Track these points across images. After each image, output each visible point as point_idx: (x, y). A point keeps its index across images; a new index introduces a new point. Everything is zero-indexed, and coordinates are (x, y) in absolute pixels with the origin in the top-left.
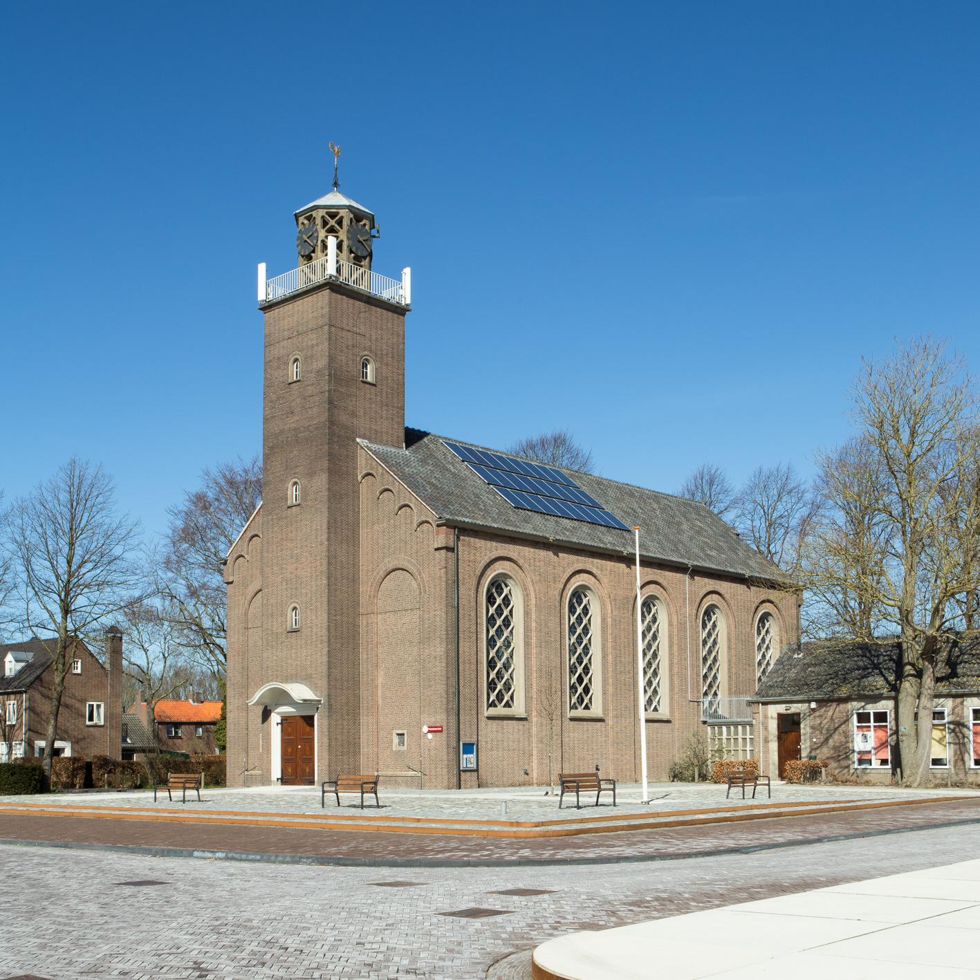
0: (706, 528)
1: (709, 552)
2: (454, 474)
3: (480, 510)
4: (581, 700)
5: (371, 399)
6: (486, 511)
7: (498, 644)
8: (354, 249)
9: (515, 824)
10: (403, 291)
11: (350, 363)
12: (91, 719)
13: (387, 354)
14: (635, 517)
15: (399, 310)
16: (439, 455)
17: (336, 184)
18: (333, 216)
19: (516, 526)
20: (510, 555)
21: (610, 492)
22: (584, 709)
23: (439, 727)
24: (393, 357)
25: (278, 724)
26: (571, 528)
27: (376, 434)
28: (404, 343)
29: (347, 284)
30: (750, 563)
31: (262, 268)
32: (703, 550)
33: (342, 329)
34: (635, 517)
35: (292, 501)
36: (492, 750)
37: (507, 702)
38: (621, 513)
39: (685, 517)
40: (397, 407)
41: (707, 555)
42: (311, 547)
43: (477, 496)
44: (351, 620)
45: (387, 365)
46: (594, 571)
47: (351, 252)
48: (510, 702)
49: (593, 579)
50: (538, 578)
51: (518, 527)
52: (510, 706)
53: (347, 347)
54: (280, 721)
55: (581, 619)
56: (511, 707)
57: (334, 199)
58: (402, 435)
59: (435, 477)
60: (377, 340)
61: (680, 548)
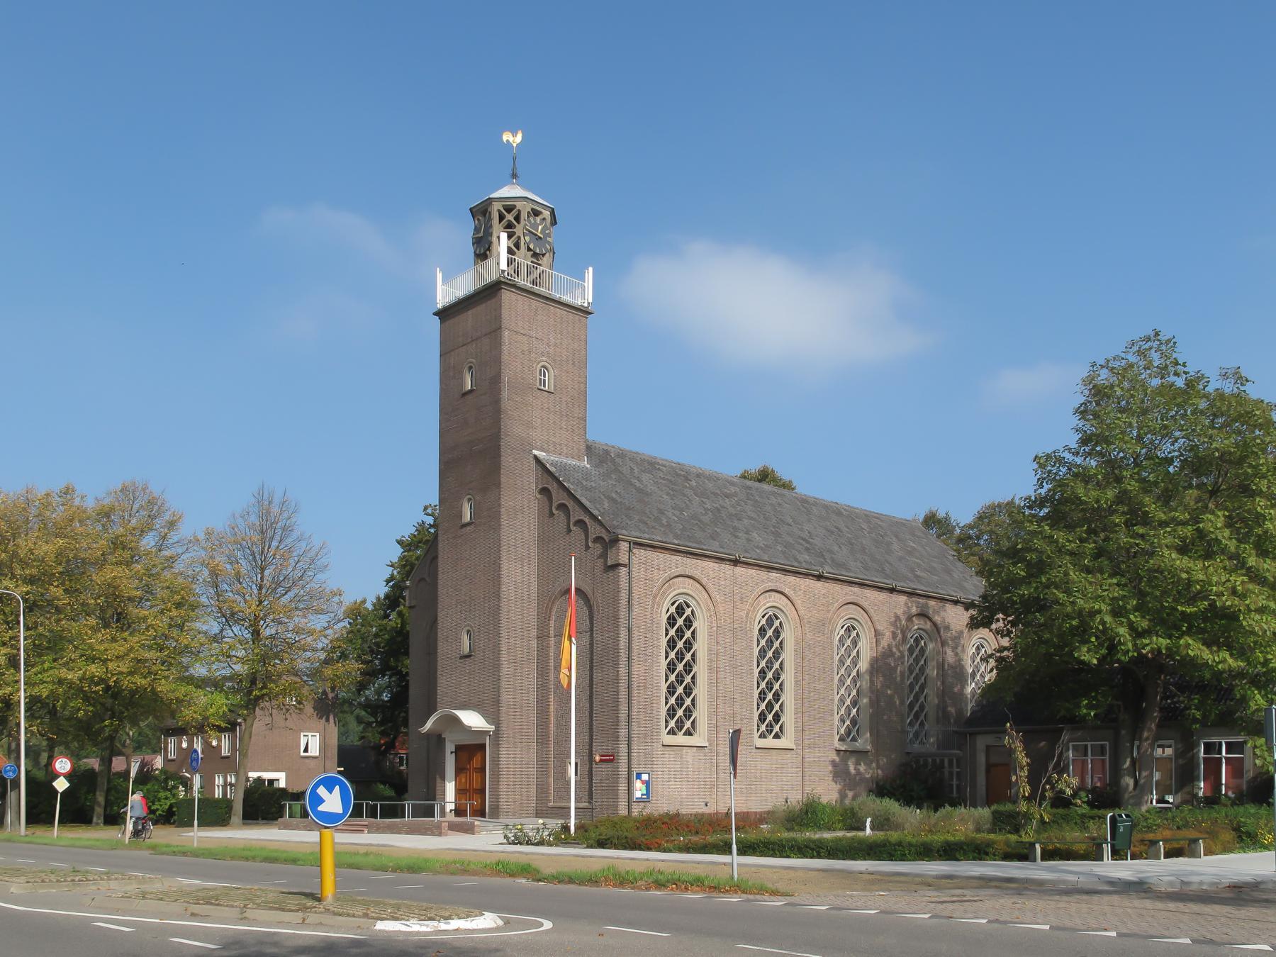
0: (919, 548)
1: (919, 573)
2: (639, 490)
3: (662, 525)
4: (770, 726)
5: (549, 408)
6: (669, 525)
7: (849, 680)
8: (532, 246)
9: (250, 858)
10: (584, 295)
11: (526, 369)
12: (306, 750)
13: (567, 361)
14: (839, 536)
15: (585, 312)
16: (625, 470)
17: (514, 176)
18: (509, 209)
19: (700, 543)
20: (696, 574)
21: (815, 510)
22: (851, 741)
23: (611, 756)
24: (574, 364)
25: (452, 753)
26: (763, 546)
27: (554, 446)
28: (586, 349)
29: (510, 280)
30: (966, 584)
31: (438, 269)
32: (912, 571)
33: (517, 332)
34: (839, 536)
35: (467, 517)
36: (669, 781)
37: (777, 733)
38: (824, 531)
39: (896, 537)
40: (579, 418)
41: (917, 577)
42: (484, 566)
43: (661, 512)
44: (525, 643)
45: (568, 372)
46: (787, 591)
47: (529, 249)
48: (780, 733)
49: (785, 599)
50: (723, 598)
51: (702, 544)
52: (690, 734)
53: (523, 352)
54: (454, 750)
55: (772, 642)
56: (692, 735)
57: (510, 191)
58: (583, 448)
59: (616, 491)
60: (555, 345)
61: (886, 569)
